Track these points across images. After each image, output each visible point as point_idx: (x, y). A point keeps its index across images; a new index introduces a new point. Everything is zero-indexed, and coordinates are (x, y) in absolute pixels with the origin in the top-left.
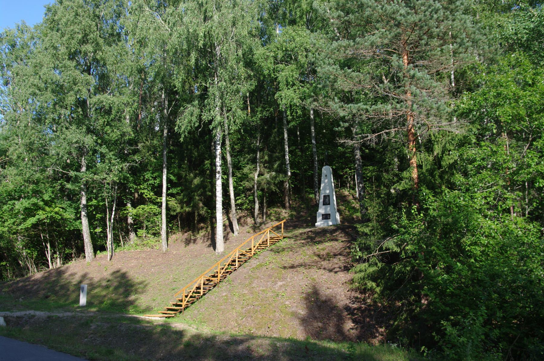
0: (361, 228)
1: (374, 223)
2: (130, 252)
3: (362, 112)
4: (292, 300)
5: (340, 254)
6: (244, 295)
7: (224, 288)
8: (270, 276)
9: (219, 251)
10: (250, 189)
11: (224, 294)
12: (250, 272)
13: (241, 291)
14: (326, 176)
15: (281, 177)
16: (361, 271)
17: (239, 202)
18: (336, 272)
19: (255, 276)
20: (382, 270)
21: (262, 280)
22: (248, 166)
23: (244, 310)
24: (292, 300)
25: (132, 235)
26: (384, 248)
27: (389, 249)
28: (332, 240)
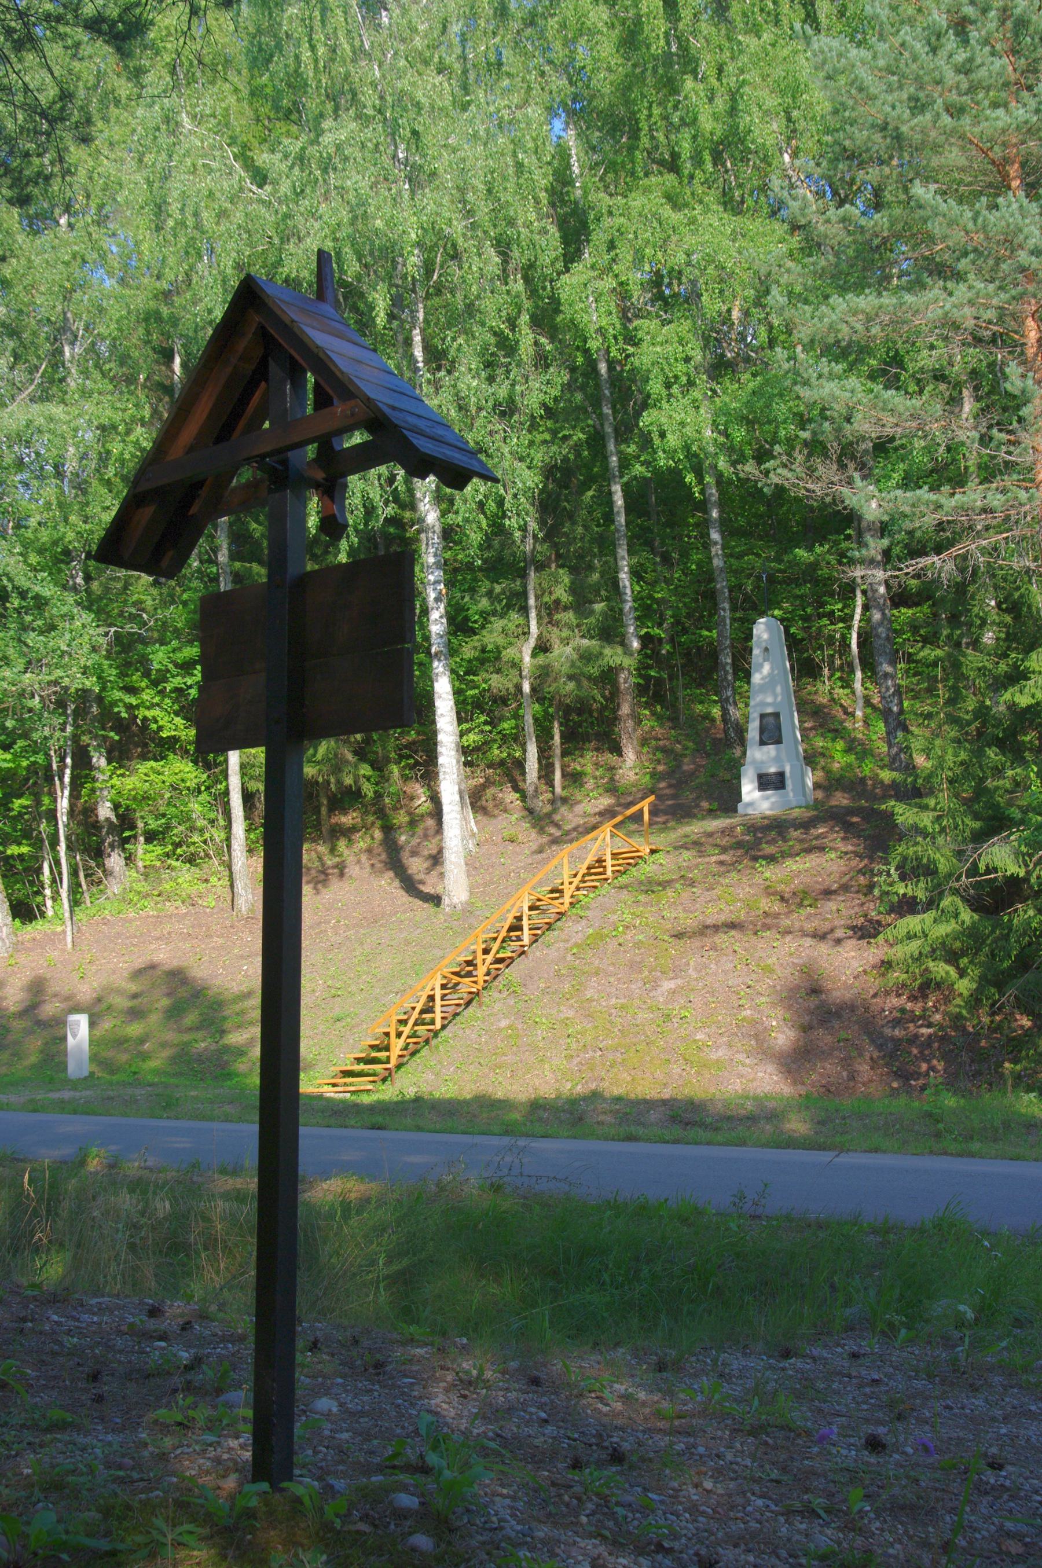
0: (905, 814)
1: (944, 799)
2: (125, 920)
3: (923, 508)
4: (713, 1028)
5: (845, 888)
6: (565, 1023)
7: (498, 1007)
8: (634, 966)
9: (455, 900)
10: (502, 700)
11: (503, 1024)
12: (569, 957)
13: (554, 1012)
14: (766, 649)
15: (613, 655)
16: (910, 937)
17: (472, 738)
18: (838, 941)
19: (586, 969)
20: (972, 934)
21: (612, 979)
22: (498, 624)
23: (576, 1061)
24: (713, 1028)
25: (115, 860)
26: (982, 867)
27: (995, 870)
28: (809, 851)
